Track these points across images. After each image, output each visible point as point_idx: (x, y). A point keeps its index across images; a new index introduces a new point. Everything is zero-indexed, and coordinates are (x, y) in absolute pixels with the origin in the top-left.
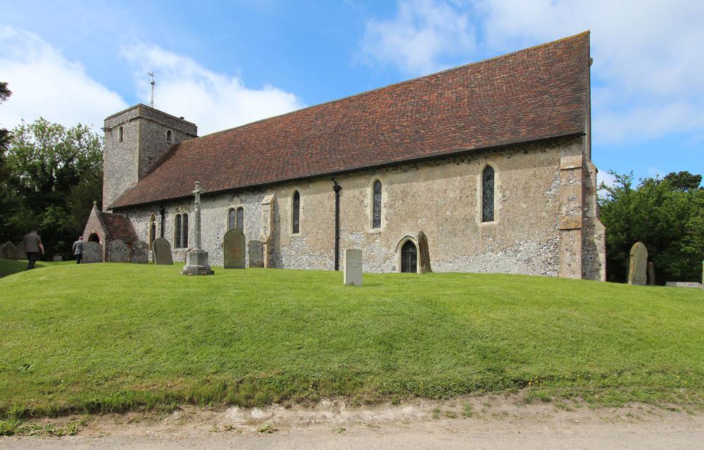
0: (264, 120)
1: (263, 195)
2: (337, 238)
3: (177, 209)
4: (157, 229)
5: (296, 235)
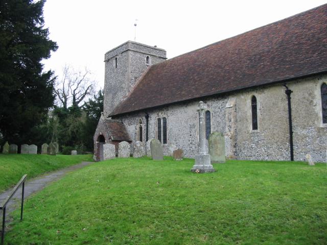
0: (219, 42)
1: (226, 100)
2: (291, 133)
3: (158, 114)
4: (143, 130)
5: (255, 131)
